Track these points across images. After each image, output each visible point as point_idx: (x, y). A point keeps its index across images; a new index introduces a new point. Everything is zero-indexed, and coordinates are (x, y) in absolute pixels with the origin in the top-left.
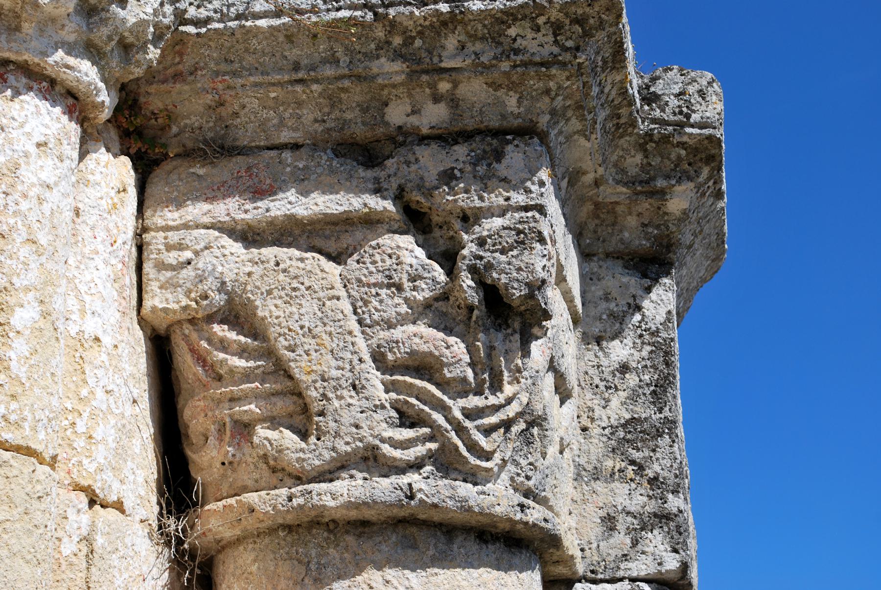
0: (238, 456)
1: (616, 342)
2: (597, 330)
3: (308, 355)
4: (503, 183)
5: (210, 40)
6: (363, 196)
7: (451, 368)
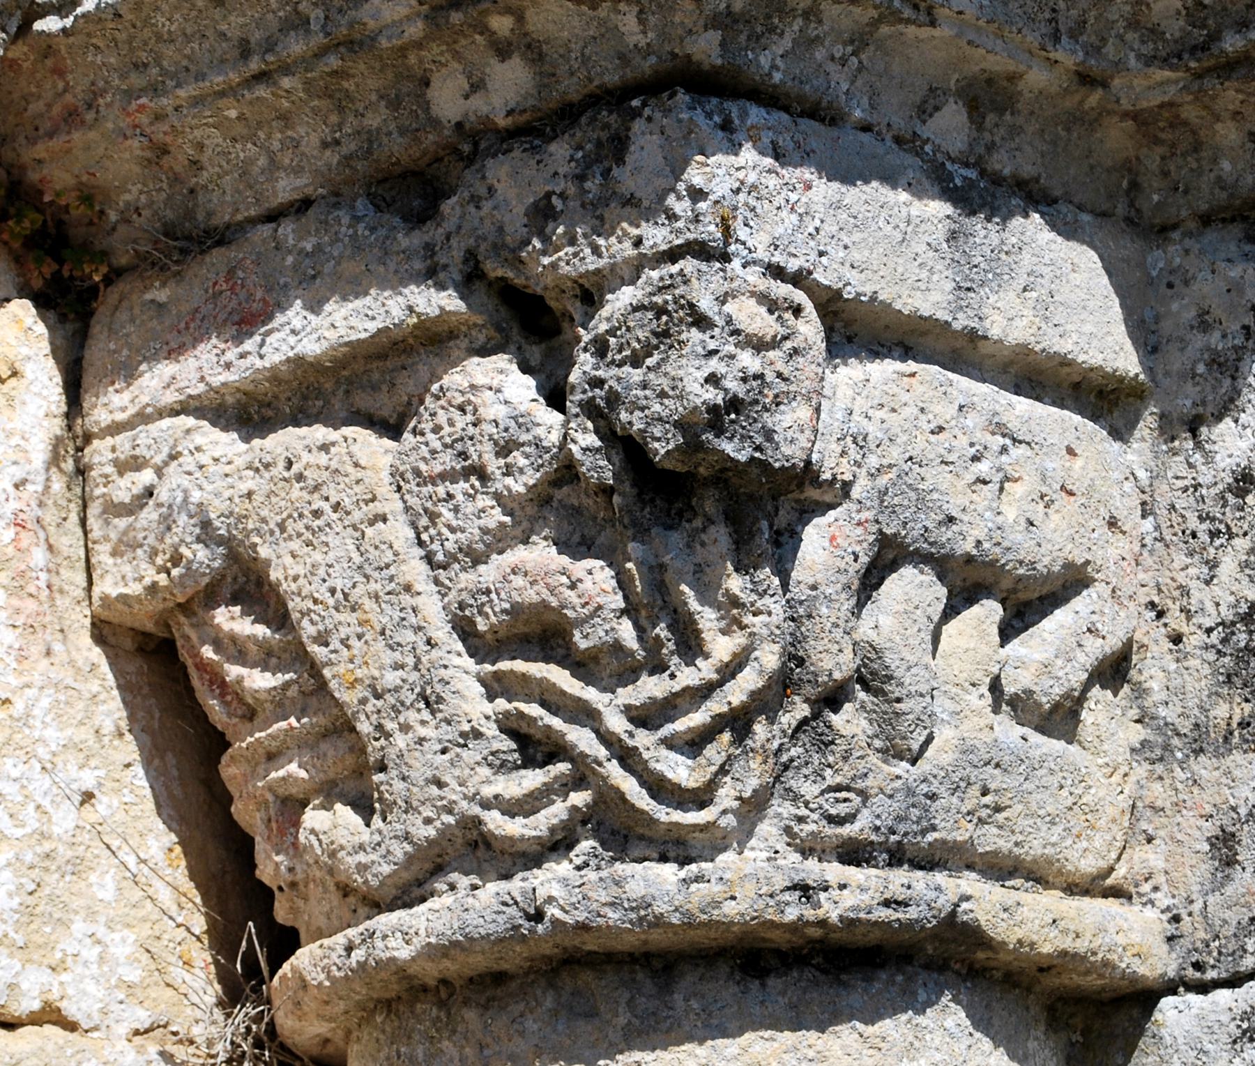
0: (298, 869)
1: (1228, 422)
2: (1188, 403)
3: (348, 647)
4: (628, 209)
5: (89, 35)
6: (406, 291)
7: (587, 629)
